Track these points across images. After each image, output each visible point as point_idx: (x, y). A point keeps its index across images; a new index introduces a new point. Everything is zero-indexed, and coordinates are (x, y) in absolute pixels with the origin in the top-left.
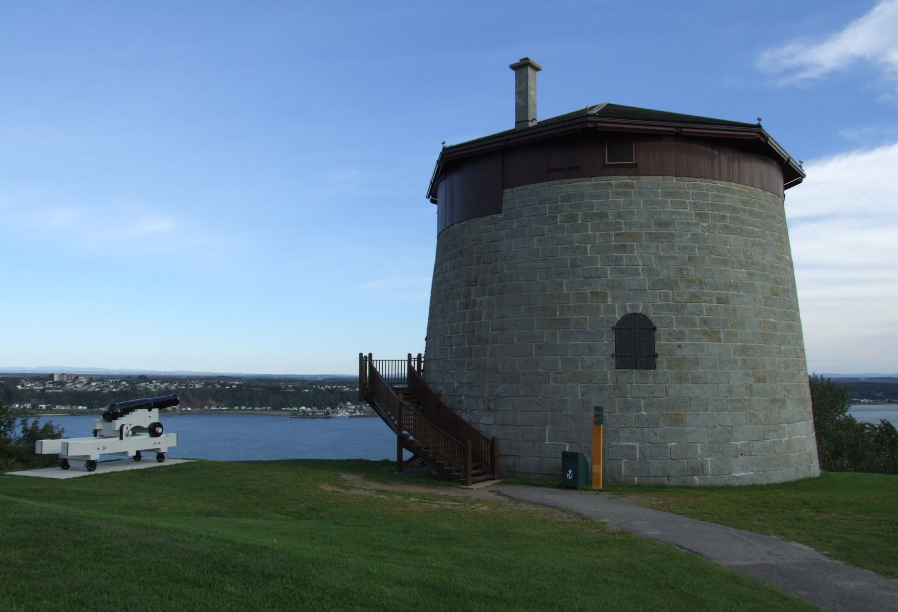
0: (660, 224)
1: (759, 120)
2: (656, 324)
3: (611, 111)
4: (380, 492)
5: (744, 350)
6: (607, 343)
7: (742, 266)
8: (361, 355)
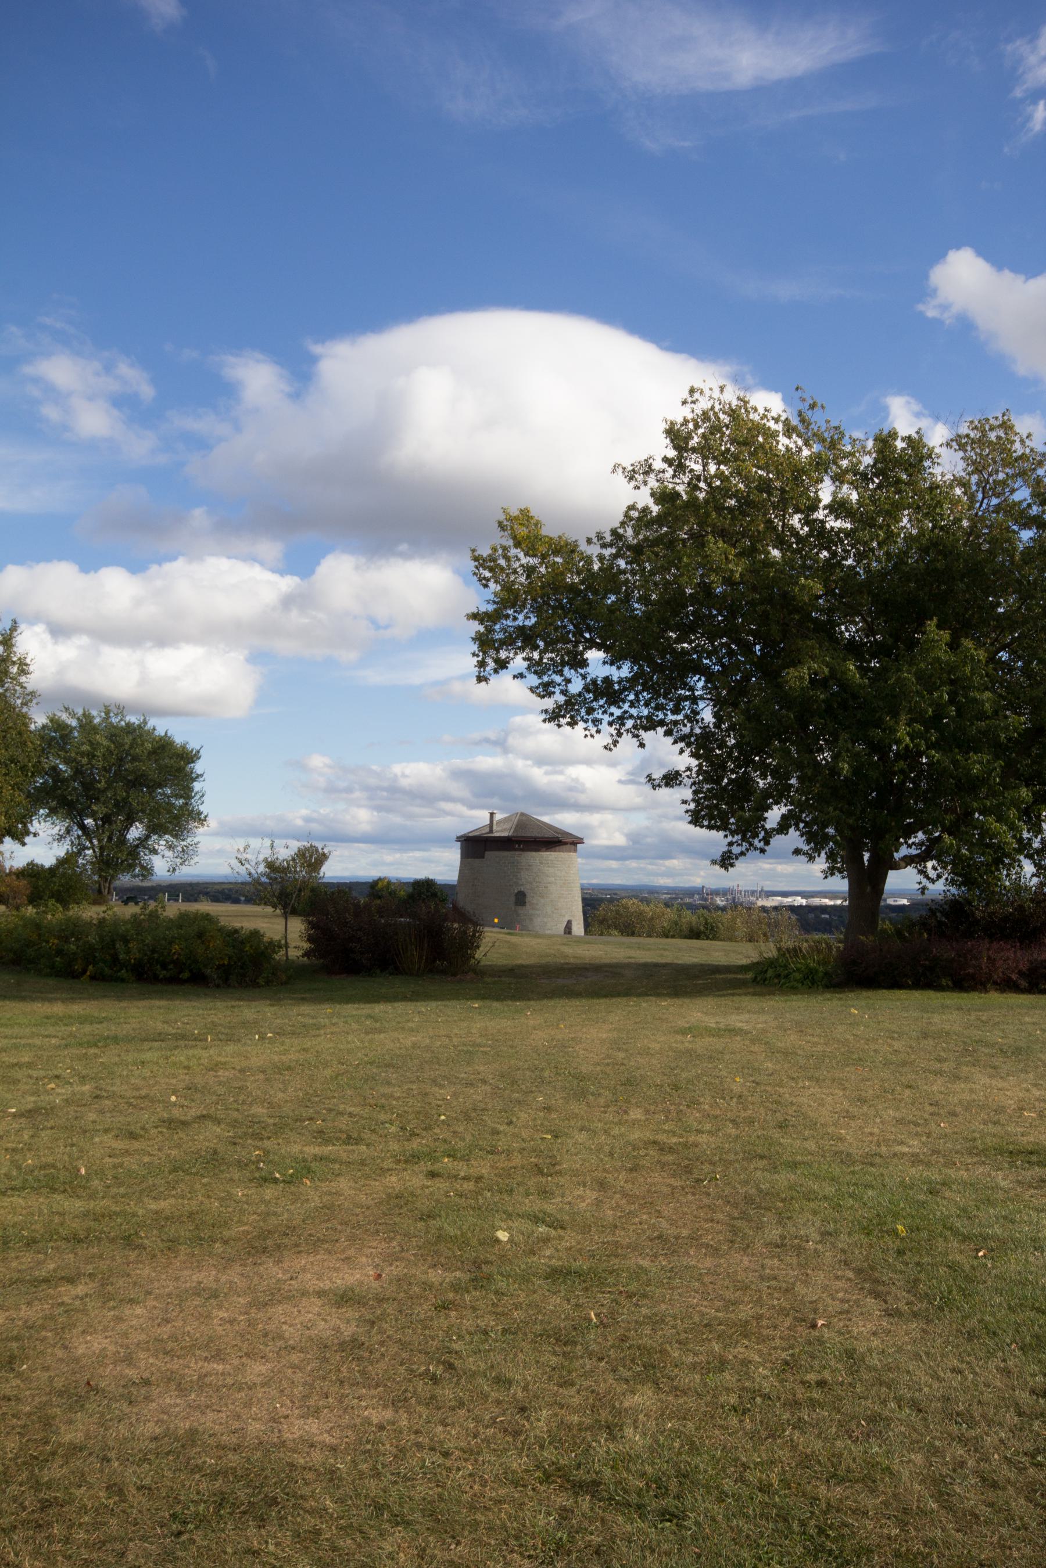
6: (513, 899)
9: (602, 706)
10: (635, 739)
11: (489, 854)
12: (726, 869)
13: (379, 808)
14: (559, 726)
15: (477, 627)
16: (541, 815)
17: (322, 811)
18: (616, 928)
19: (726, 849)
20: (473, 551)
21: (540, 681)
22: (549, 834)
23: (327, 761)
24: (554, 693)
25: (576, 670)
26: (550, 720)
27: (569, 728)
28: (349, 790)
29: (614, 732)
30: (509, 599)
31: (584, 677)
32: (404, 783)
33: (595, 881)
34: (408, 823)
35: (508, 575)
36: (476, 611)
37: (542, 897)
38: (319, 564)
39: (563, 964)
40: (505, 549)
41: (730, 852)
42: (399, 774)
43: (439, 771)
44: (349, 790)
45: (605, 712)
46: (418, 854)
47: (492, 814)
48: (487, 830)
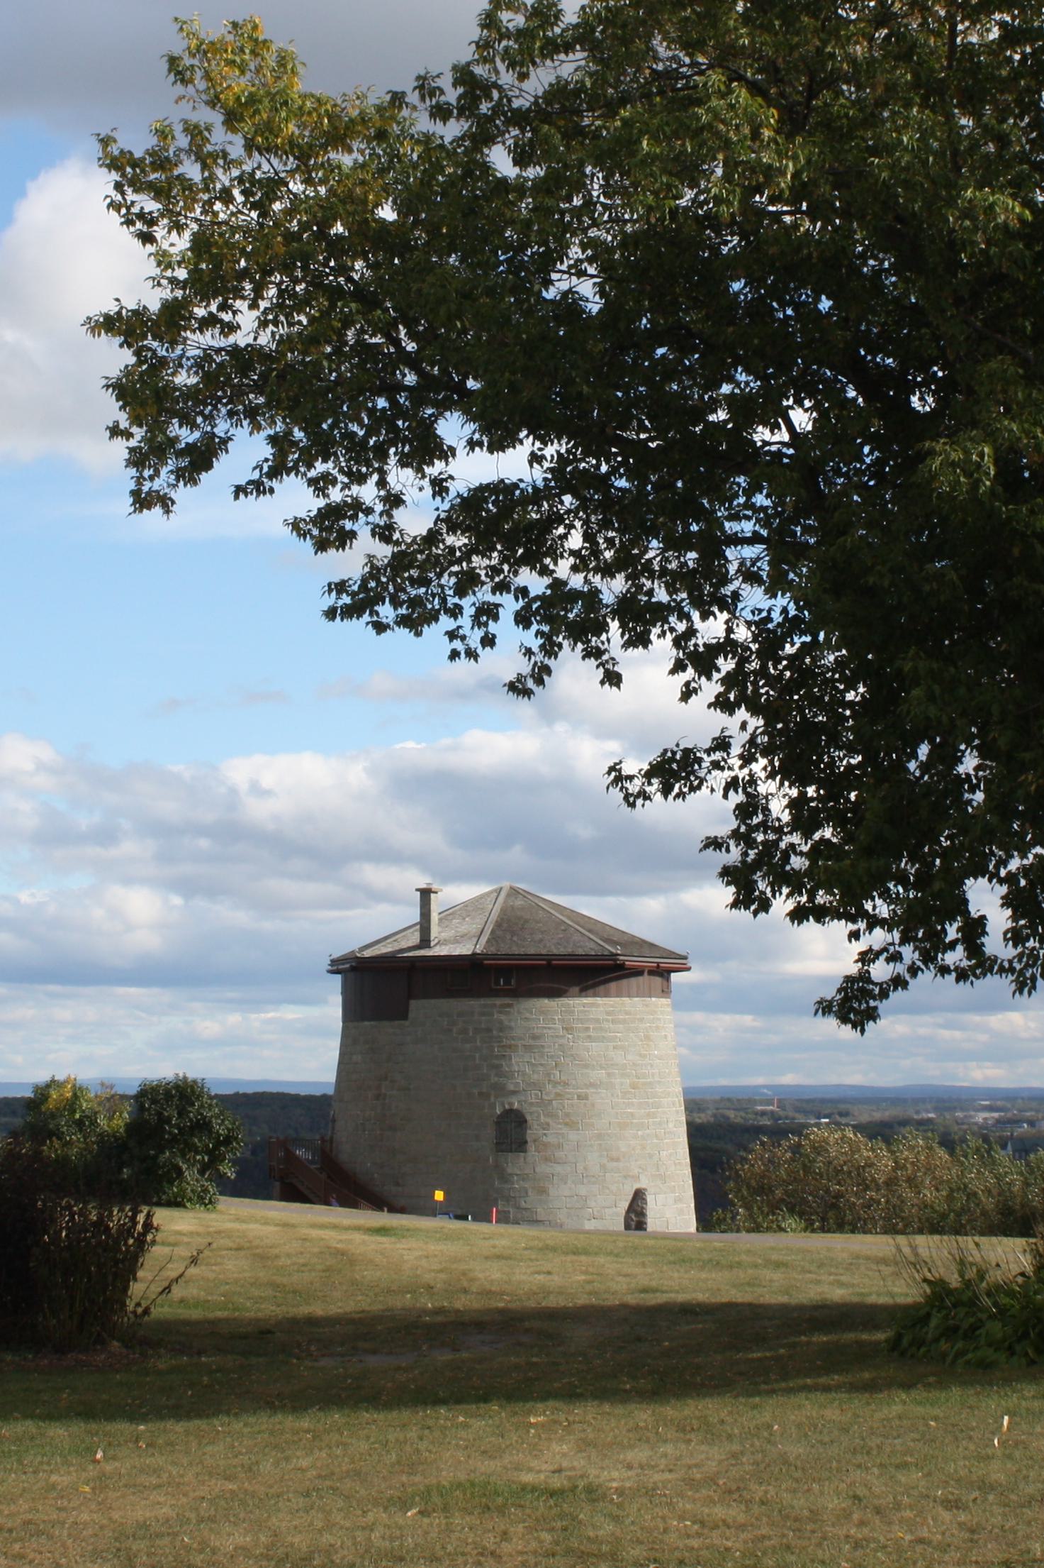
2: (528, 1118)
4: (382, 1231)
5: (600, 1136)
6: (490, 1132)
7: (602, 1068)
9: (495, 570)
10: (592, 662)
11: (418, 1007)
12: (859, 1025)
13: (187, 887)
14: (380, 627)
15: (116, 357)
16: (598, 890)
17: (24, 897)
18: (792, 1211)
19: (854, 969)
20: (105, 142)
21: (321, 502)
22: (588, 946)
23: (46, 753)
24: (353, 535)
25: (419, 470)
26: (351, 612)
27: (403, 633)
28: (106, 836)
29: (535, 644)
30: (212, 273)
31: (439, 487)
32: (259, 811)
33: (789, 1079)
34: (268, 925)
35: (208, 207)
36: (112, 308)
37: (571, 1125)
38: (22, 193)
39: (383, 1311)
40: (196, 132)
41: (864, 977)
42: (244, 787)
43: (357, 775)
44: (106, 836)
45: (502, 587)
46: (291, 1013)
47: (426, 894)
48: (415, 938)
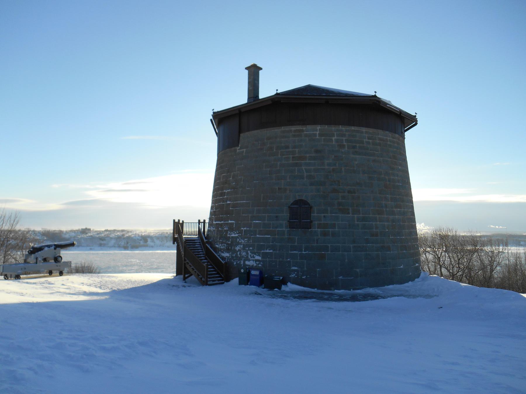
0: (317, 151)
1: (375, 92)
3: (309, 89)
6: (286, 214)
8: (174, 220)
